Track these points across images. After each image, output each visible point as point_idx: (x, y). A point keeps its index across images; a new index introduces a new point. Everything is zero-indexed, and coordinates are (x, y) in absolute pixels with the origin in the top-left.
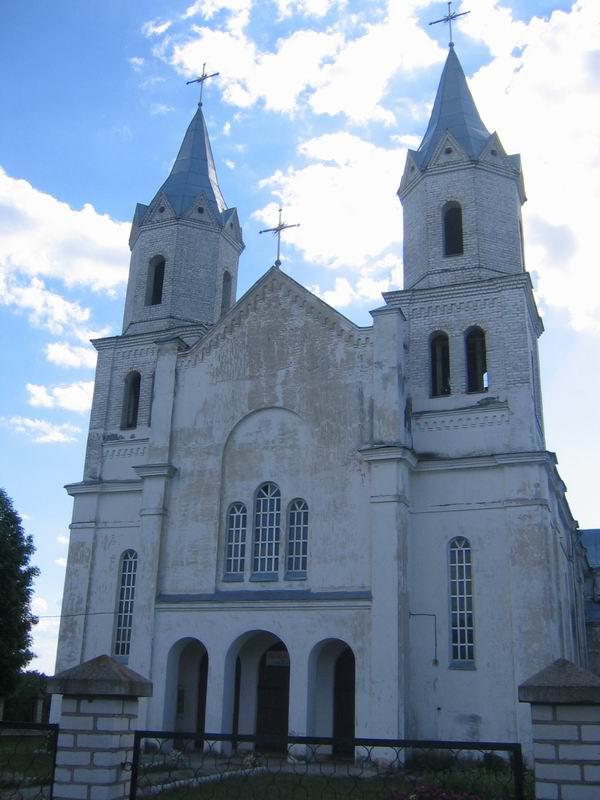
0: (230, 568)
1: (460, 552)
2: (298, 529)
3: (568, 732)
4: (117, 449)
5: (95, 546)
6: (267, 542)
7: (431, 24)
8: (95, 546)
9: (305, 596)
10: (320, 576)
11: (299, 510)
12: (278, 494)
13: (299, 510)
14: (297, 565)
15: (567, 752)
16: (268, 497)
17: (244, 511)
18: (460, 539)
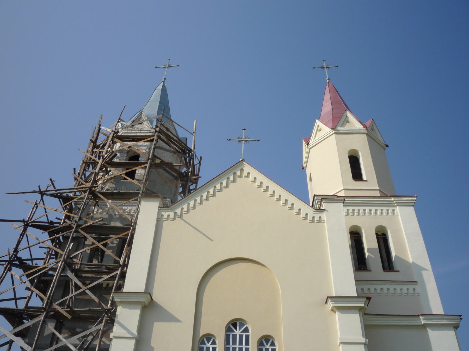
12: (246, 330)
17: (214, 343)
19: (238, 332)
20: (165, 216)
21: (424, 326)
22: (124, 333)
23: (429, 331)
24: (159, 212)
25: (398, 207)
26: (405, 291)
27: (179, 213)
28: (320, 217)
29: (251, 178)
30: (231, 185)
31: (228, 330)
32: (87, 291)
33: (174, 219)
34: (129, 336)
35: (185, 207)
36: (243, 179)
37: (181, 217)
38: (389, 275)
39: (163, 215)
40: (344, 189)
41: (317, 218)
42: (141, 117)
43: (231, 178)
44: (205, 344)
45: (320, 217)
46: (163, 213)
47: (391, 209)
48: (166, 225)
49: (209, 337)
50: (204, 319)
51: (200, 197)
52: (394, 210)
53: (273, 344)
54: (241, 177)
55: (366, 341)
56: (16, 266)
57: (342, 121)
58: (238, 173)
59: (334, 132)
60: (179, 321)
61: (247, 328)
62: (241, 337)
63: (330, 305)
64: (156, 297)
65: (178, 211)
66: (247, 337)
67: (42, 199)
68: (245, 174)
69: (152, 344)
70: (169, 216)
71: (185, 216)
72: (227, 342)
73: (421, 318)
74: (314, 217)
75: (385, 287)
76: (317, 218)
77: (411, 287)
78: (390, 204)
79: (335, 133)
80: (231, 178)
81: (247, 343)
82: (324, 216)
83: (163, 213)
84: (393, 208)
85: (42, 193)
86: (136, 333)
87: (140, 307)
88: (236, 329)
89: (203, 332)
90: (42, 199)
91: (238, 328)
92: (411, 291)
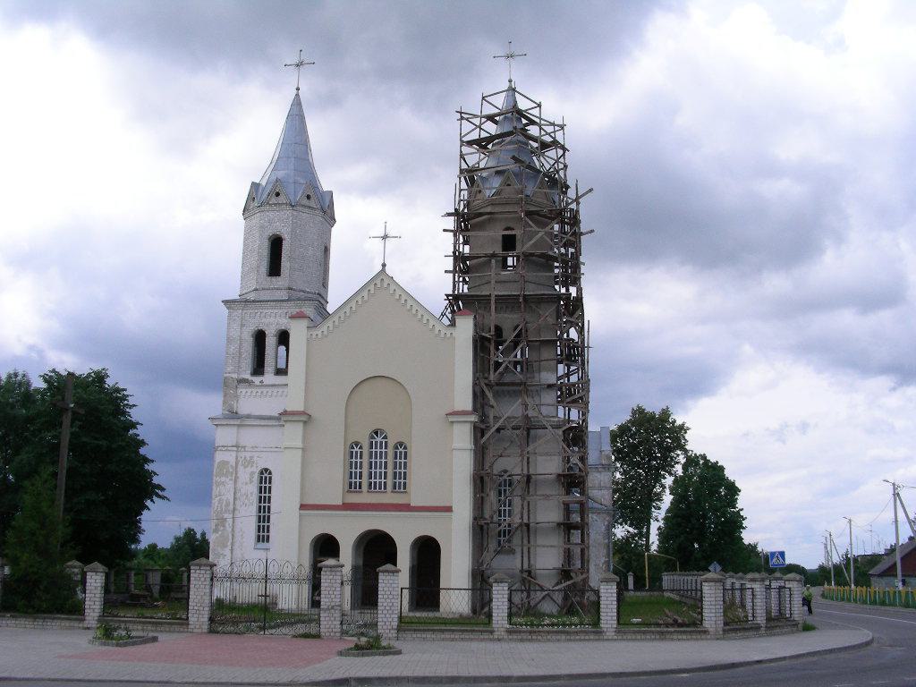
0: (353, 487)
1: (266, 478)
2: (400, 463)
3: (501, 588)
4: (249, 391)
5: (237, 464)
6: (378, 470)
7: (591, 190)
8: (237, 464)
9: (406, 508)
10: (416, 497)
11: (356, 449)
12: (385, 437)
13: (356, 449)
14: (401, 485)
15: (609, 591)
16: (379, 439)
17: (361, 448)
18: (266, 470)
62: (381, 443)
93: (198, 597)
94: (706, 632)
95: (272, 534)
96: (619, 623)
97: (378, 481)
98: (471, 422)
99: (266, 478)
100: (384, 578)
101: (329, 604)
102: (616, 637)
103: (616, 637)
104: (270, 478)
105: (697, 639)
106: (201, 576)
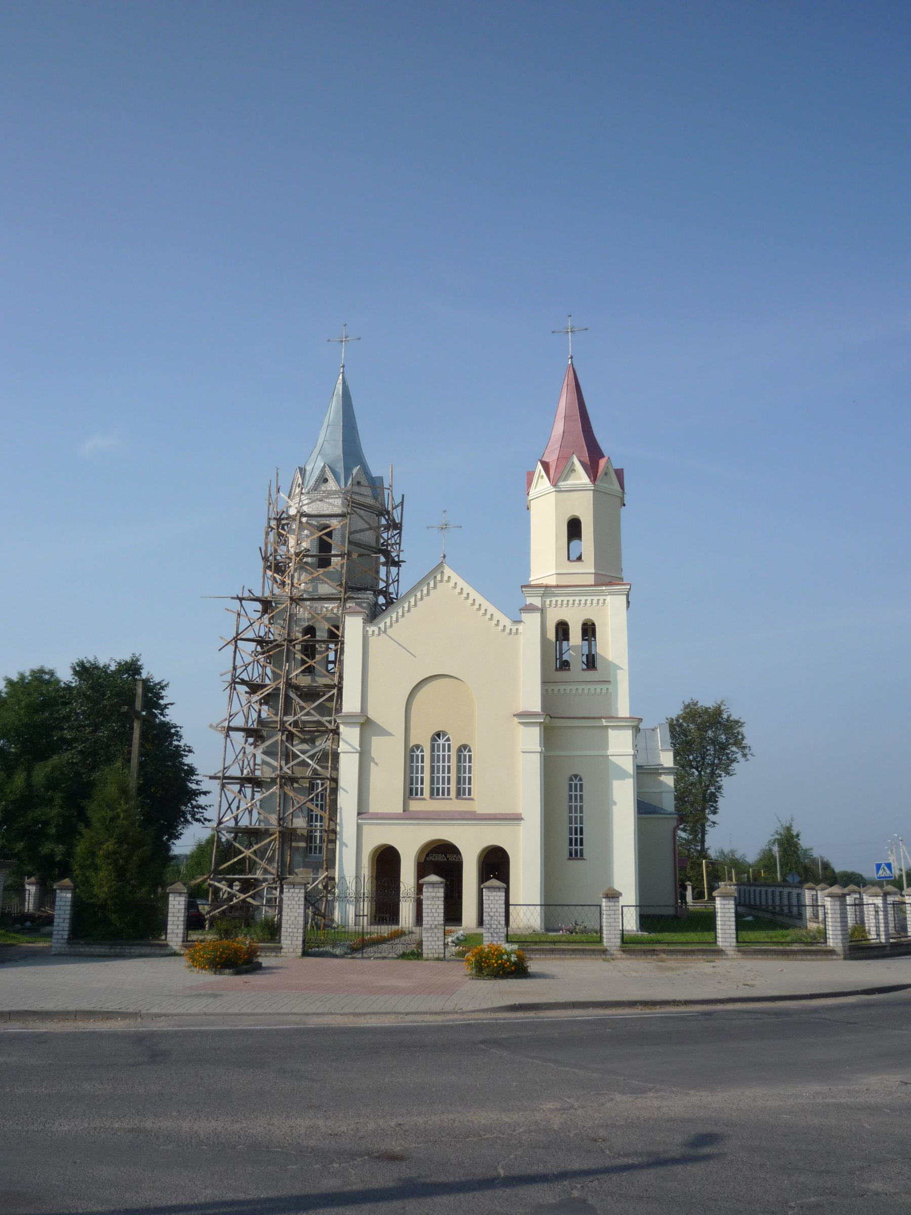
0: (411, 792)
1: (576, 785)
10: (480, 803)
12: (448, 740)
15: (727, 906)
17: (422, 751)
18: (576, 776)
19: (441, 741)
20: (370, 633)
21: (607, 727)
22: (350, 749)
23: (610, 730)
24: (364, 627)
25: (609, 596)
26: (598, 691)
27: (383, 629)
28: (517, 629)
29: (452, 584)
30: (432, 592)
31: (433, 739)
32: (312, 711)
33: (379, 634)
34: (355, 751)
35: (388, 620)
36: (444, 584)
37: (385, 632)
38: (591, 675)
39: (367, 631)
40: (556, 574)
41: (514, 631)
42: (325, 471)
43: (432, 584)
44: (415, 752)
45: (517, 629)
46: (368, 629)
47: (602, 598)
48: (372, 641)
49: (418, 747)
50: (413, 732)
51: (401, 609)
52: (605, 600)
53: (470, 751)
54: (441, 581)
55: (542, 749)
56: (238, 683)
57: (566, 472)
58: (439, 578)
59: (554, 489)
60: (394, 736)
61: (448, 738)
62: (444, 745)
63: (516, 720)
64: (371, 714)
65: (382, 625)
66: (449, 745)
67: (242, 605)
68: (446, 578)
69: (373, 755)
70: (373, 631)
71: (389, 630)
72: (433, 750)
73: (603, 720)
74: (511, 629)
75: (580, 687)
76: (514, 631)
77: (604, 687)
78: (601, 593)
79: (555, 491)
80: (432, 584)
81: (449, 751)
82: (521, 627)
83: (368, 629)
84: (604, 597)
85: (241, 599)
86: (359, 749)
87: (359, 725)
88: (440, 739)
89: (412, 744)
90: (242, 605)
91: (441, 738)
92: (604, 691)
93: (292, 918)
94: (604, 951)
95: (585, 847)
96: (738, 942)
97: (441, 786)
98: (541, 723)
99: (576, 785)
100: (489, 894)
101: (430, 923)
102: (735, 957)
103: (735, 957)
104: (581, 785)
105: (802, 960)
106: (295, 895)
